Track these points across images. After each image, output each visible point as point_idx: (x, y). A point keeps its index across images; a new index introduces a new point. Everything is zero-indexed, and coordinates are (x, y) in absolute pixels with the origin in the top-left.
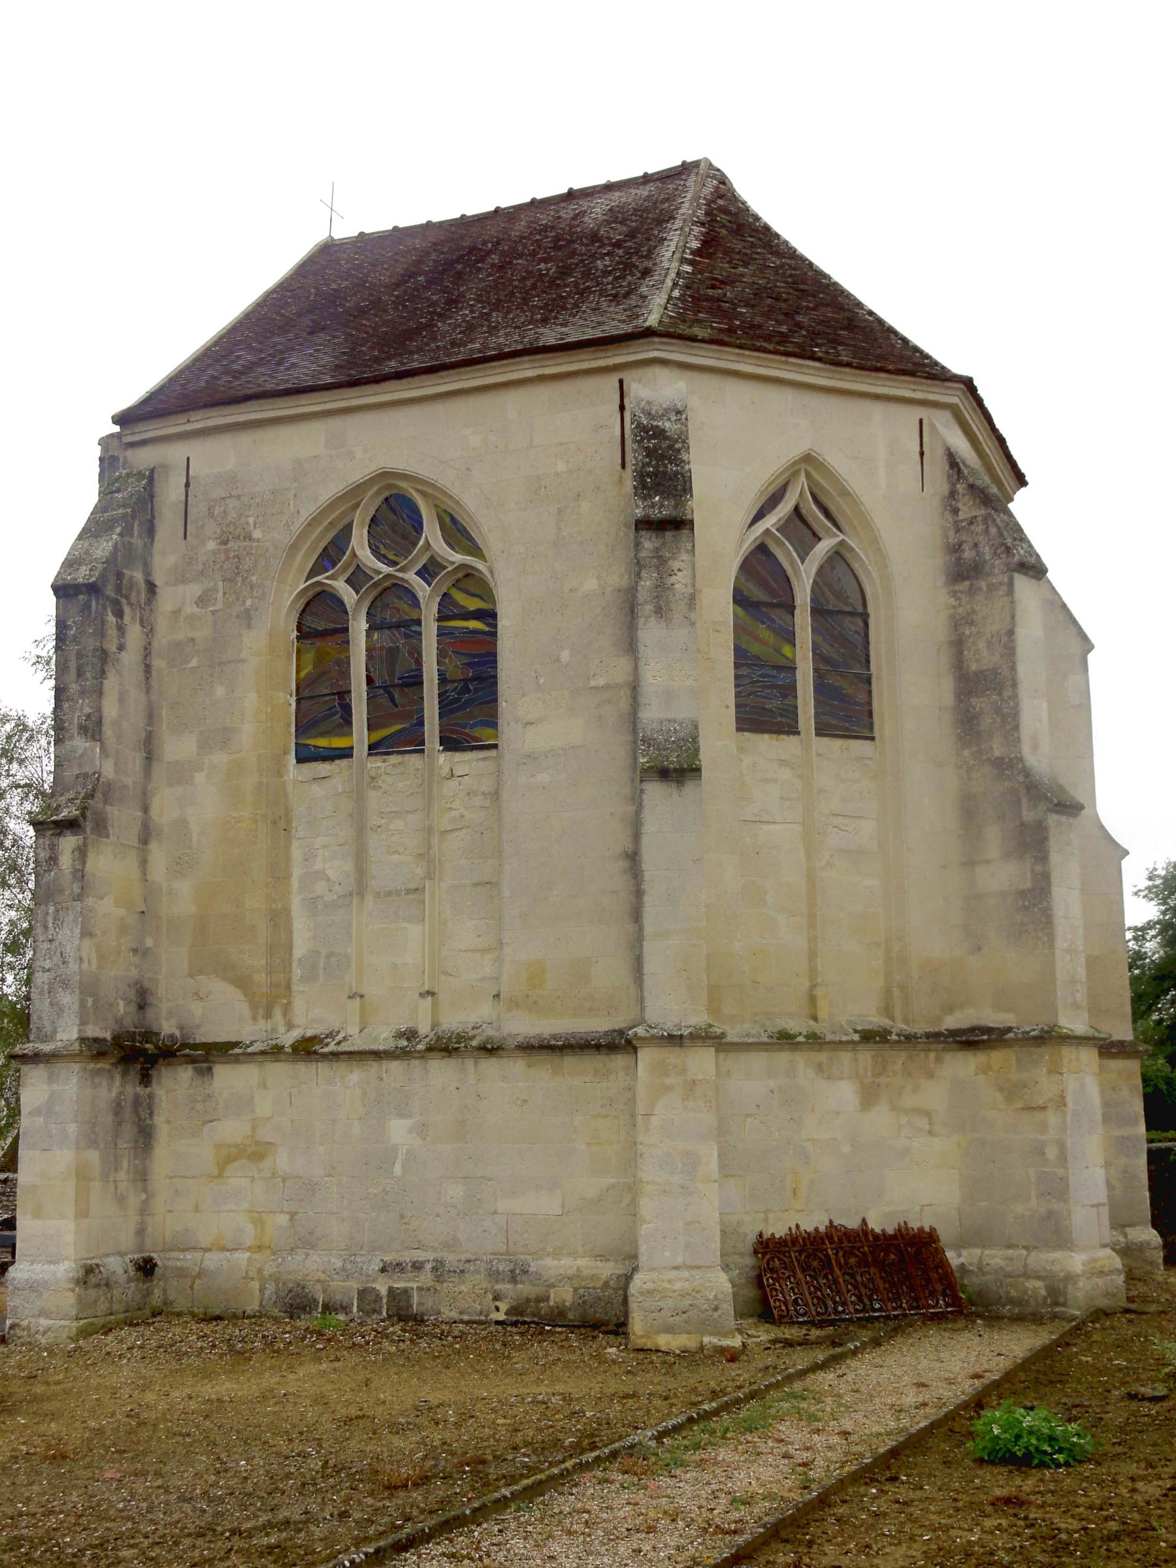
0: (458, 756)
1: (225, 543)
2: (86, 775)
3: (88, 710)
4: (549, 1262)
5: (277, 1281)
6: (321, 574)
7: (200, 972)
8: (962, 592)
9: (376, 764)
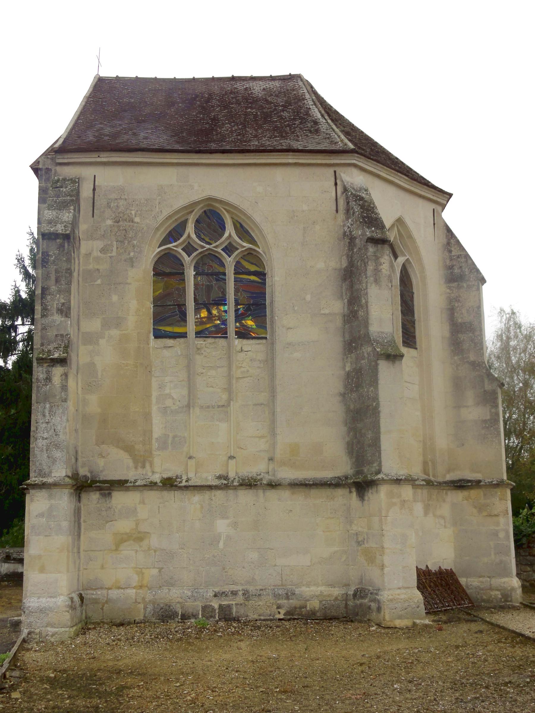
0: (245, 341)
1: (118, 222)
2: (62, 335)
3: (63, 301)
4: (304, 589)
5: (154, 603)
6: (171, 243)
7: (103, 443)
8: (453, 287)
9: (200, 342)
